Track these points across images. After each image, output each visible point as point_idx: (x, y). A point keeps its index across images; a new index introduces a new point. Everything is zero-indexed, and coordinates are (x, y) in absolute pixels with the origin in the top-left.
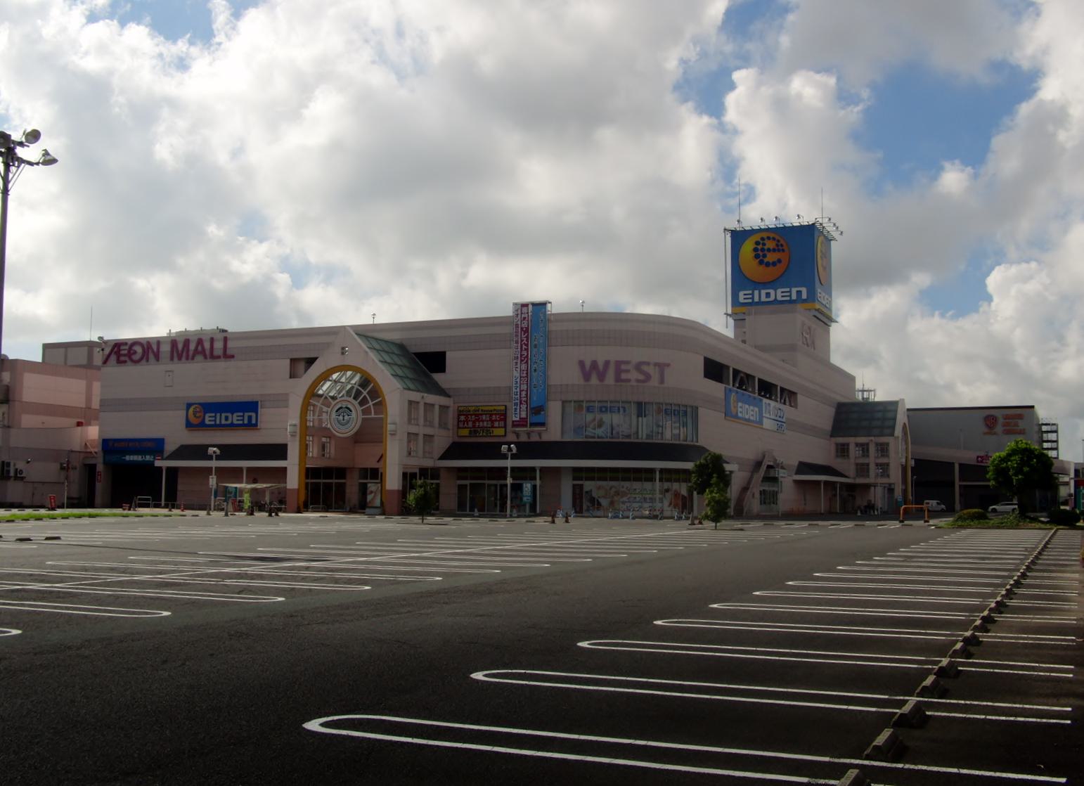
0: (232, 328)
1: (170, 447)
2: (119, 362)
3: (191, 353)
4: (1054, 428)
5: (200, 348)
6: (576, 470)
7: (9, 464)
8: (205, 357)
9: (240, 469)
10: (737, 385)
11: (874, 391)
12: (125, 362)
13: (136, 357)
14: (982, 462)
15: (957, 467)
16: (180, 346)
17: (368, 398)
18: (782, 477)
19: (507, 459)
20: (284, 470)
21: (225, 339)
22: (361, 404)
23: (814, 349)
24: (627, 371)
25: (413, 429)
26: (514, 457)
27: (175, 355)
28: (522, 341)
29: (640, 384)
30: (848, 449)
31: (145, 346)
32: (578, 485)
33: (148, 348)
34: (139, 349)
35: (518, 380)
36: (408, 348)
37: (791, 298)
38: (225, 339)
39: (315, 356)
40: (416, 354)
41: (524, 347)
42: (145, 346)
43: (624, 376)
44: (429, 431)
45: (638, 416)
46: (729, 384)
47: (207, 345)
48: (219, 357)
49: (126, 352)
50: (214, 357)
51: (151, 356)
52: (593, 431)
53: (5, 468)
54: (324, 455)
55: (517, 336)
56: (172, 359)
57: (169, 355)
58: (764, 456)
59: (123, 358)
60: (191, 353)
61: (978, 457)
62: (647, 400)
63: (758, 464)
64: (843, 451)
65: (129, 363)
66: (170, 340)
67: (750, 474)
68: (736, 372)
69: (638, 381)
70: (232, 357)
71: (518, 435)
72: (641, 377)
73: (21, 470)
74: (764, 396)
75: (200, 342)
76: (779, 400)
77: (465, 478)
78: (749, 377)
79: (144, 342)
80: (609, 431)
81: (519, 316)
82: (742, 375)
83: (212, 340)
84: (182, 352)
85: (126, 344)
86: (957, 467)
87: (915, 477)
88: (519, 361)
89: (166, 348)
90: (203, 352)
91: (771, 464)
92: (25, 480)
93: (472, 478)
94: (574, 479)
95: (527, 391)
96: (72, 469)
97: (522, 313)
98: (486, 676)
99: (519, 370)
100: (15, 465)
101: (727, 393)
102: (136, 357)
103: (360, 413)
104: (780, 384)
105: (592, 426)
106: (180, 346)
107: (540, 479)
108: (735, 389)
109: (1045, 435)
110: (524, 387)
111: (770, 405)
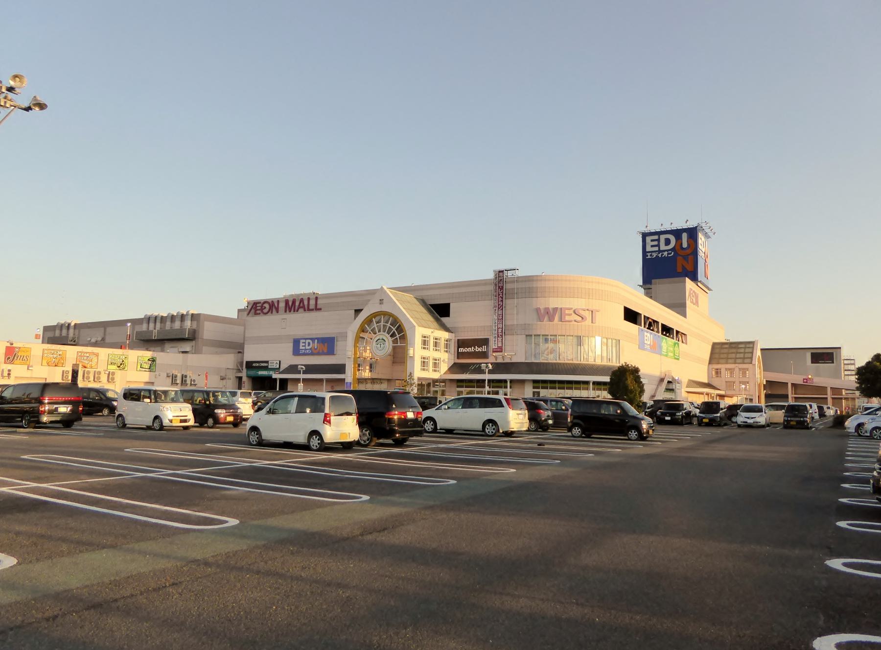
0: (320, 291)
1: (284, 366)
2: (256, 314)
3: (296, 308)
4: (852, 362)
5: (301, 305)
6: (535, 381)
7: (186, 376)
8: (305, 310)
10: (647, 326)
12: (260, 314)
13: (265, 311)
14: (806, 382)
15: (790, 386)
16: (290, 304)
17: (396, 333)
18: (678, 389)
19: (485, 373)
20: (827, 398)
21: (317, 298)
22: (392, 336)
23: (698, 307)
24: (570, 315)
25: (426, 353)
26: (490, 372)
27: (287, 309)
28: (499, 295)
29: (576, 323)
30: (720, 372)
31: (271, 303)
32: (536, 392)
33: (273, 305)
34: (267, 306)
35: (496, 321)
38: (317, 298)
39: (362, 308)
40: (430, 305)
41: (500, 299)
42: (271, 303)
43: (567, 318)
46: (640, 325)
47: (306, 303)
48: (312, 310)
49: (259, 308)
50: (309, 310)
52: (547, 356)
53: (184, 379)
55: (496, 292)
56: (286, 311)
57: (284, 309)
58: (666, 375)
60: (296, 308)
61: (804, 379)
63: (662, 380)
64: (718, 372)
65: (262, 314)
66: (284, 299)
67: (656, 386)
68: (646, 318)
69: (575, 321)
70: (320, 309)
71: (496, 358)
72: (579, 319)
73: (194, 380)
74: (665, 335)
75: (302, 301)
76: (675, 338)
77: (462, 387)
79: (270, 301)
81: (497, 278)
82: (650, 320)
83: (309, 299)
84: (292, 307)
85: (259, 303)
87: (765, 391)
88: (497, 309)
89: (282, 305)
90: (304, 307)
91: (671, 380)
92: (197, 386)
93: (466, 387)
94: (534, 388)
95: (502, 328)
96: (228, 379)
97: (499, 277)
98: (845, 565)
99: (497, 314)
100: (190, 377)
101: (641, 331)
102: (265, 311)
103: (391, 342)
104: (675, 328)
105: (546, 352)
106: (290, 304)
107: (511, 387)
108: (646, 329)
109: (846, 366)
110: (500, 326)
111: (667, 342)
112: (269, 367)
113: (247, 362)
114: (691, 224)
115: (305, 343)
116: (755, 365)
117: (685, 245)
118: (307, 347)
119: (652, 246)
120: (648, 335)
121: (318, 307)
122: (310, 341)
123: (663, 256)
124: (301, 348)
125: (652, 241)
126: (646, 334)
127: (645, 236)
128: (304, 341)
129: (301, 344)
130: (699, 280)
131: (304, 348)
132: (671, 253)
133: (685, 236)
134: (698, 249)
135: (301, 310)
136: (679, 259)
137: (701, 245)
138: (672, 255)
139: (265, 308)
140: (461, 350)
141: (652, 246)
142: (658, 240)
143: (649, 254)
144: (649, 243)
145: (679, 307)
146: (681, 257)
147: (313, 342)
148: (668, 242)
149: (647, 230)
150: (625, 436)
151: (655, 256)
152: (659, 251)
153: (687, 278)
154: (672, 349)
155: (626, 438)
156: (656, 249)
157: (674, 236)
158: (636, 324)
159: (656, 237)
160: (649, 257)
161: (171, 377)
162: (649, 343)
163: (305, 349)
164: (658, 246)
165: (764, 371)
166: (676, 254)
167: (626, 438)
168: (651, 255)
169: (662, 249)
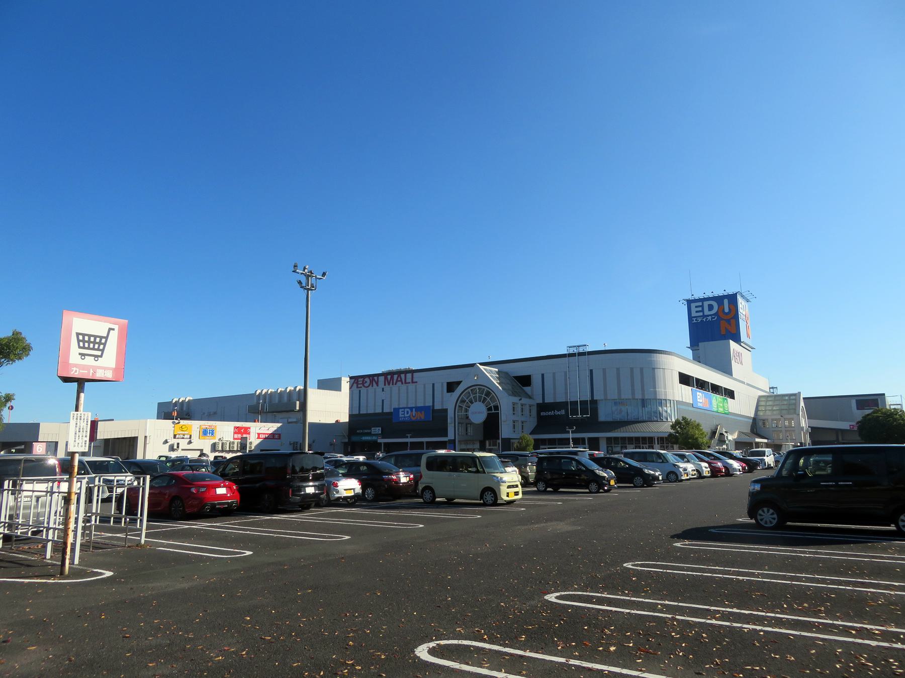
3: (395, 381)
5: (399, 379)
8: (402, 383)
9: (422, 443)
11: (777, 388)
27: (387, 383)
36: (510, 374)
37: (703, 313)
39: (461, 380)
40: (514, 377)
44: (523, 419)
45: (642, 407)
49: (361, 382)
51: (374, 383)
54: (467, 434)
59: (359, 386)
60: (395, 381)
61: (850, 425)
62: (600, 399)
68: (698, 380)
78: (705, 382)
80: (626, 415)
86: (754, 444)
90: (401, 381)
102: (367, 385)
112: (372, 433)
113: (309, 423)
114: (730, 291)
115: (404, 411)
116: (799, 414)
117: (727, 310)
118: (406, 415)
119: (697, 312)
120: (700, 394)
121: (414, 381)
122: (408, 410)
123: (708, 320)
124: (401, 416)
125: (696, 307)
126: (698, 393)
127: (689, 302)
128: (403, 410)
129: (401, 413)
130: (742, 341)
131: (403, 416)
132: (714, 318)
133: (726, 301)
134: (739, 313)
135: (399, 384)
136: (723, 322)
137: (742, 308)
138: (715, 319)
139: (366, 382)
140: (543, 414)
141: (697, 312)
142: (702, 306)
143: (694, 319)
144: (694, 309)
145: (726, 370)
146: (724, 321)
147: (412, 411)
148: (711, 307)
149: (691, 298)
150: (586, 489)
151: (700, 320)
152: (704, 316)
153: (731, 341)
154: (721, 405)
155: (587, 491)
156: (701, 314)
157: (717, 303)
158: (689, 386)
159: (700, 304)
160: (695, 321)
161: (292, 445)
162: (701, 401)
163: (405, 417)
164: (703, 311)
165: (808, 419)
166: (720, 319)
167: (587, 491)
168: (696, 320)
169: (705, 314)
